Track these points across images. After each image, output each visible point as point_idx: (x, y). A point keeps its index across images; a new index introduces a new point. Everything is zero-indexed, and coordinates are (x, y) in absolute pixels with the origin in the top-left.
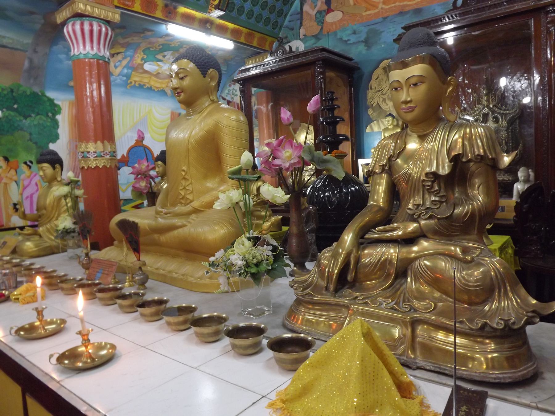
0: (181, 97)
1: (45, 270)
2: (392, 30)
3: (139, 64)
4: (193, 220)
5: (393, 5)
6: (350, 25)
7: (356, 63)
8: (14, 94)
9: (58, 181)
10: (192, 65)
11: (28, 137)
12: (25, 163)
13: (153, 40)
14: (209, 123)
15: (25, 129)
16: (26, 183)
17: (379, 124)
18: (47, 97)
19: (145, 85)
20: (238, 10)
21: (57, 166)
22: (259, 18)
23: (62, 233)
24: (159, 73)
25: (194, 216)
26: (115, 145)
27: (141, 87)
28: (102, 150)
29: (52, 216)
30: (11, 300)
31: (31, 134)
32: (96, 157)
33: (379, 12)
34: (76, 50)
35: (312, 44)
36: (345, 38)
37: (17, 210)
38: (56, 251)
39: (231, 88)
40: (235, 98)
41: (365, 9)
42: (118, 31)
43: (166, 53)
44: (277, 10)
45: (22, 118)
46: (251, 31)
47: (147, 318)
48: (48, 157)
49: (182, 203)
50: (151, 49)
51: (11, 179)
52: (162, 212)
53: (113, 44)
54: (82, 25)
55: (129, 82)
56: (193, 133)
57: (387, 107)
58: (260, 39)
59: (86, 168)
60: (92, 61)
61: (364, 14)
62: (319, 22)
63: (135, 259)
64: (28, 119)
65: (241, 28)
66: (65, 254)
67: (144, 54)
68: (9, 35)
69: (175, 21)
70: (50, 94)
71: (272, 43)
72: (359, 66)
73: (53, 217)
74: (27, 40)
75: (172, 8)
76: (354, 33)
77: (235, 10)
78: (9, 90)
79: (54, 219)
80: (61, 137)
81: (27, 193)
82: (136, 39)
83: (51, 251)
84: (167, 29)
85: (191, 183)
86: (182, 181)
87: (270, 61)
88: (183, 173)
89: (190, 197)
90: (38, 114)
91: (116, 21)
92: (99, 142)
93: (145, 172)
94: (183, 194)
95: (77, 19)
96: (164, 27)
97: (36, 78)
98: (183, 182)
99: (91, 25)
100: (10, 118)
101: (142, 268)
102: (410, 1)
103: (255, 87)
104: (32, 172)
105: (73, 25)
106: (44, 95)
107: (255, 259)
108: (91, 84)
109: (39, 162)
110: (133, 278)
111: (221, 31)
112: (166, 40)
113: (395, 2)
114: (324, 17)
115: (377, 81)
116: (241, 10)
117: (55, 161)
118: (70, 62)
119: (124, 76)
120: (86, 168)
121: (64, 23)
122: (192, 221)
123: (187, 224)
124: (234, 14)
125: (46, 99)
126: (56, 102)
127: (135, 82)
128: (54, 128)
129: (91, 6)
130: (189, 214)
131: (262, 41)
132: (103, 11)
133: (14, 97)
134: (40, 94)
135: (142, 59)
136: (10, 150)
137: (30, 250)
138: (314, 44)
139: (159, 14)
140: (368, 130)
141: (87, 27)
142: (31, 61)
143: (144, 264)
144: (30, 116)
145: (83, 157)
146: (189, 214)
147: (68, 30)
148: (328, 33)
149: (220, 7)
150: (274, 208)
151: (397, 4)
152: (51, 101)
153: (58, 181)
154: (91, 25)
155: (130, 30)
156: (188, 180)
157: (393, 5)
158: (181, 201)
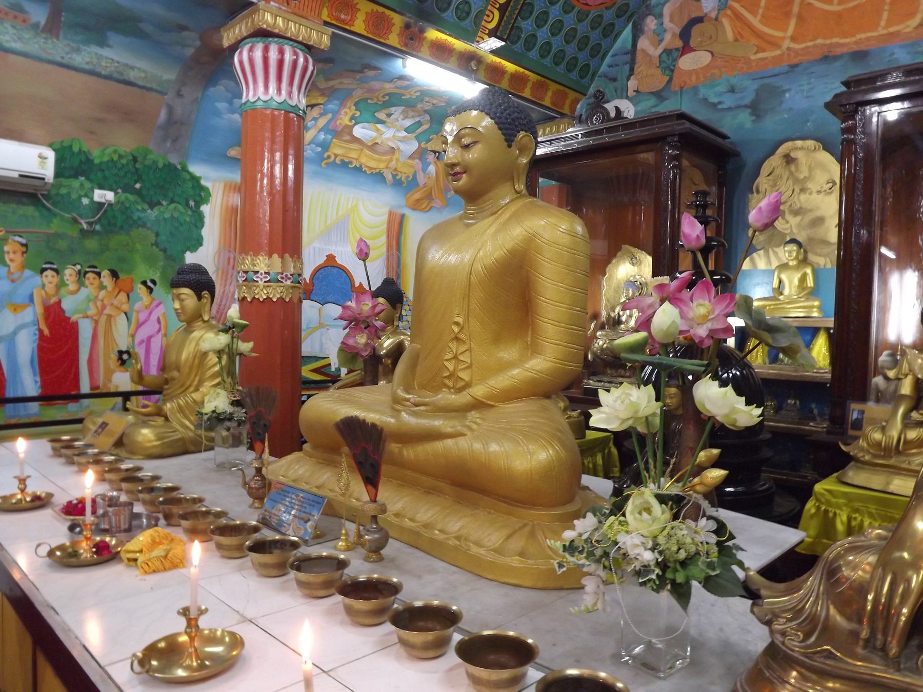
0: (461, 183)
2: (806, 88)
3: (346, 126)
4: (475, 423)
5: (810, 44)
6: (724, 76)
7: (731, 143)
8: (137, 166)
9: (204, 322)
10: (487, 121)
11: (153, 239)
12: (144, 283)
13: (376, 85)
14: (517, 233)
15: (149, 225)
16: (142, 317)
17: (768, 257)
19: (351, 163)
20: (526, 40)
21: (205, 294)
22: (559, 58)
23: (208, 419)
25: (474, 415)
26: (302, 264)
27: (345, 165)
29: (188, 384)
30: (121, 560)
31: (157, 234)
32: (269, 281)
33: (782, 55)
34: (251, 93)
35: (650, 106)
37: (123, 363)
38: (192, 448)
41: (756, 49)
42: (320, 65)
43: (393, 109)
45: (146, 207)
46: (543, 79)
47: (415, 653)
48: (192, 277)
49: (449, 388)
51: (118, 308)
52: (408, 400)
53: (311, 88)
54: (266, 50)
56: (481, 253)
57: (788, 226)
58: (555, 93)
59: (249, 300)
60: (276, 113)
61: (753, 57)
62: (665, 68)
63: (366, 498)
65: (527, 72)
66: (210, 454)
68: (139, 64)
69: (419, 54)
70: (196, 169)
71: (576, 102)
72: (738, 149)
73: (190, 386)
74: (168, 75)
76: (732, 90)
77: (522, 41)
78: (131, 158)
79: (192, 389)
80: (205, 243)
81: (142, 334)
82: (347, 82)
84: (404, 66)
85: (470, 350)
86: (450, 345)
87: (570, 135)
88: (456, 329)
89: (465, 375)
90: (172, 201)
92: (275, 256)
93: (367, 317)
94: (451, 368)
95: (258, 39)
96: (399, 62)
97: (175, 141)
98: (453, 346)
99: (281, 52)
100: (127, 205)
102: (846, 37)
103: (542, 177)
104: (153, 299)
105: (251, 50)
106: (184, 169)
107: (682, 551)
108: (272, 153)
109: (175, 284)
112: (397, 87)
114: (675, 60)
115: (769, 178)
117: (200, 282)
119: (318, 145)
120: (249, 300)
121: (235, 47)
122: (475, 427)
123: (465, 430)
124: (519, 46)
125: (188, 177)
126: (203, 182)
127: (336, 156)
128: (196, 226)
129: (284, 18)
130: (462, 410)
131: (559, 98)
132: (303, 29)
133: (137, 169)
134: (179, 167)
135: (352, 118)
136: (122, 260)
137: (149, 445)
139: (393, 39)
140: (746, 265)
141: (273, 55)
144: (159, 204)
146: (462, 410)
147: (241, 57)
148: (682, 88)
150: (718, 433)
151: (819, 41)
152: (196, 180)
153: (204, 322)
154: (281, 52)
155: (342, 67)
156: (464, 342)
157: (810, 44)
158: (447, 381)
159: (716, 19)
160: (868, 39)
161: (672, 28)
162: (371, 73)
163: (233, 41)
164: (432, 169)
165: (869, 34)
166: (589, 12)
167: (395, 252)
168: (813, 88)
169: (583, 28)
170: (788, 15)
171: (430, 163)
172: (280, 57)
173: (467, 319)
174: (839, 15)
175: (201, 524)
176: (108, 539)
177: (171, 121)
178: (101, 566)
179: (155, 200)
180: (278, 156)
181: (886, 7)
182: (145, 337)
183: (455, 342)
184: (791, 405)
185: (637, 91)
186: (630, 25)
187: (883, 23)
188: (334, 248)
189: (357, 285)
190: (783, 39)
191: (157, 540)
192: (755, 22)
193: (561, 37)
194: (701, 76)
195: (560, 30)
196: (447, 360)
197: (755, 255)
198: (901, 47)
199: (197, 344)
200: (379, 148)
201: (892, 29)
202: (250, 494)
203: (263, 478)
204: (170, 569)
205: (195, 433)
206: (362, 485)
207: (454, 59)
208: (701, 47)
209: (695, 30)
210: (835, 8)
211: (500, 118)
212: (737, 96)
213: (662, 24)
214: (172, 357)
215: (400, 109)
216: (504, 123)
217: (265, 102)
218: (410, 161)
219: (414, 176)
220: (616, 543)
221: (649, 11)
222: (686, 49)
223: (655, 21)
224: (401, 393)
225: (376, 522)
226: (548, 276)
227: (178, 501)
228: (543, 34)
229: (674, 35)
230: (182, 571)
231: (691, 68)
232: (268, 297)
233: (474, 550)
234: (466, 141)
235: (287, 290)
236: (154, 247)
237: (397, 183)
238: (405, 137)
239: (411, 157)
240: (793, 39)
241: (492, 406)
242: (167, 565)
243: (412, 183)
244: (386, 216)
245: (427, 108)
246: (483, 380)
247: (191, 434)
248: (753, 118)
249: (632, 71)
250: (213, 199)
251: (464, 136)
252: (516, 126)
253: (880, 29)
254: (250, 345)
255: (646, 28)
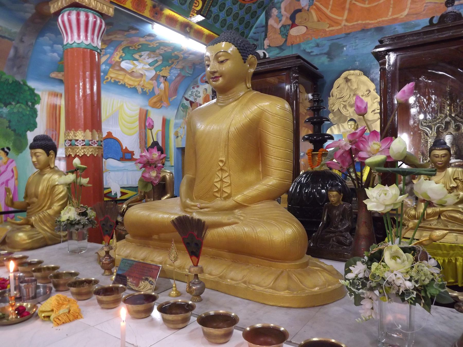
1: (29, 260)
3: (117, 62)
4: (242, 216)
6: (313, 39)
9: (51, 168)
12: (3, 149)
13: (135, 39)
15: (4, 116)
17: (339, 128)
18: (29, 87)
20: (214, 17)
21: (52, 152)
24: (133, 71)
25: (237, 211)
28: (91, 139)
29: (44, 205)
31: (10, 121)
33: (342, 28)
36: (309, 50)
38: (50, 242)
39: (194, 90)
40: (198, 99)
41: (328, 25)
43: (143, 53)
44: (245, 22)
48: (43, 142)
50: (130, 48)
52: (196, 206)
54: (78, 15)
55: (106, 78)
57: (348, 112)
60: (85, 50)
61: (327, 30)
64: (8, 107)
65: (214, 34)
67: (123, 53)
69: (160, 22)
70: (32, 84)
74: (15, 29)
75: (159, 9)
76: (318, 45)
79: (46, 208)
83: (43, 243)
84: (153, 28)
88: (221, 164)
89: (228, 190)
90: (18, 102)
91: (110, 15)
92: (88, 131)
93: (156, 161)
95: (73, 8)
97: (19, 68)
98: (220, 174)
99: (87, 16)
101: (199, 276)
102: (372, 20)
104: (8, 159)
105: (69, 14)
106: (25, 84)
110: (190, 287)
111: (198, 35)
112: (146, 41)
113: (357, 21)
114: (288, 30)
115: (338, 89)
116: (216, 18)
118: (55, 55)
121: (58, 13)
122: (242, 218)
124: (211, 21)
125: (27, 88)
126: (36, 92)
127: (111, 78)
128: (33, 117)
134: (22, 83)
135: (121, 57)
137: (24, 242)
138: (278, 54)
141: (82, 17)
142: (16, 49)
143: (202, 271)
144: (10, 104)
145: (70, 145)
148: (292, 45)
149: (202, 13)
151: (360, 22)
152: (32, 91)
153: (51, 168)
154: (87, 16)
155: (121, 26)
159: (308, 10)
160: (383, 21)
161: (286, 15)
162: (133, 32)
163: (57, 9)
164: (162, 85)
165: (384, 19)
166: (245, 4)
167: (143, 130)
168: (357, 45)
169: (242, 13)
170: (344, 9)
171: (161, 83)
172: (86, 19)
173: (227, 158)
174: (368, 9)
175: (85, 289)
176: (25, 304)
177: (17, 56)
178: (27, 321)
179: (8, 101)
180: (88, 73)
181: (391, 6)
182: (5, 180)
183: (220, 172)
184: (354, 200)
185: (269, 46)
186: (264, 13)
187: (390, 14)
188: (111, 128)
189: (124, 148)
190: (342, 20)
191: (61, 302)
192: (328, 12)
193: (231, 17)
194: (302, 38)
195: (231, 13)
196: (216, 182)
197: (332, 127)
198: (399, 25)
199: (49, 181)
200: (135, 74)
201: (395, 16)
202: (103, 267)
203: (110, 257)
204: (73, 320)
205: (51, 234)
206: (188, 256)
207: (178, 26)
208: (301, 24)
209: (298, 15)
210: (367, 6)
211: (239, 46)
212: (320, 48)
213: (280, 12)
214: (32, 190)
215: (147, 53)
216: (241, 49)
217: (78, 44)
218: (151, 81)
219: (153, 89)
220: (383, 279)
221: (274, 6)
222: (293, 25)
223: (277, 11)
224: (188, 202)
225: (198, 278)
226: (272, 132)
227: (58, 276)
228: (222, 15)
229: (287, 18)
230: (81, 320)
231: (296, 35)
232: (84, 154)
233: (257, 288)
234: (221, 59)
235: (95, 150)
236: (8, 129)
237: (144, 93)
238: (148, 68)
239: (152, 79)
240: (347, 20)
241: (247, 206)
242: (71, 318)
243: (152, 93)
244: (138, 111)
245: (161, 53)
246: (238, 192)
247: (49, 234)
248: (329, 59)
249: (266, 36)
250: (42, 101)
251: (220, 56)
252: (248, 51)
253: (389, 16)
254: (88, 179)
255: (272, 14)
